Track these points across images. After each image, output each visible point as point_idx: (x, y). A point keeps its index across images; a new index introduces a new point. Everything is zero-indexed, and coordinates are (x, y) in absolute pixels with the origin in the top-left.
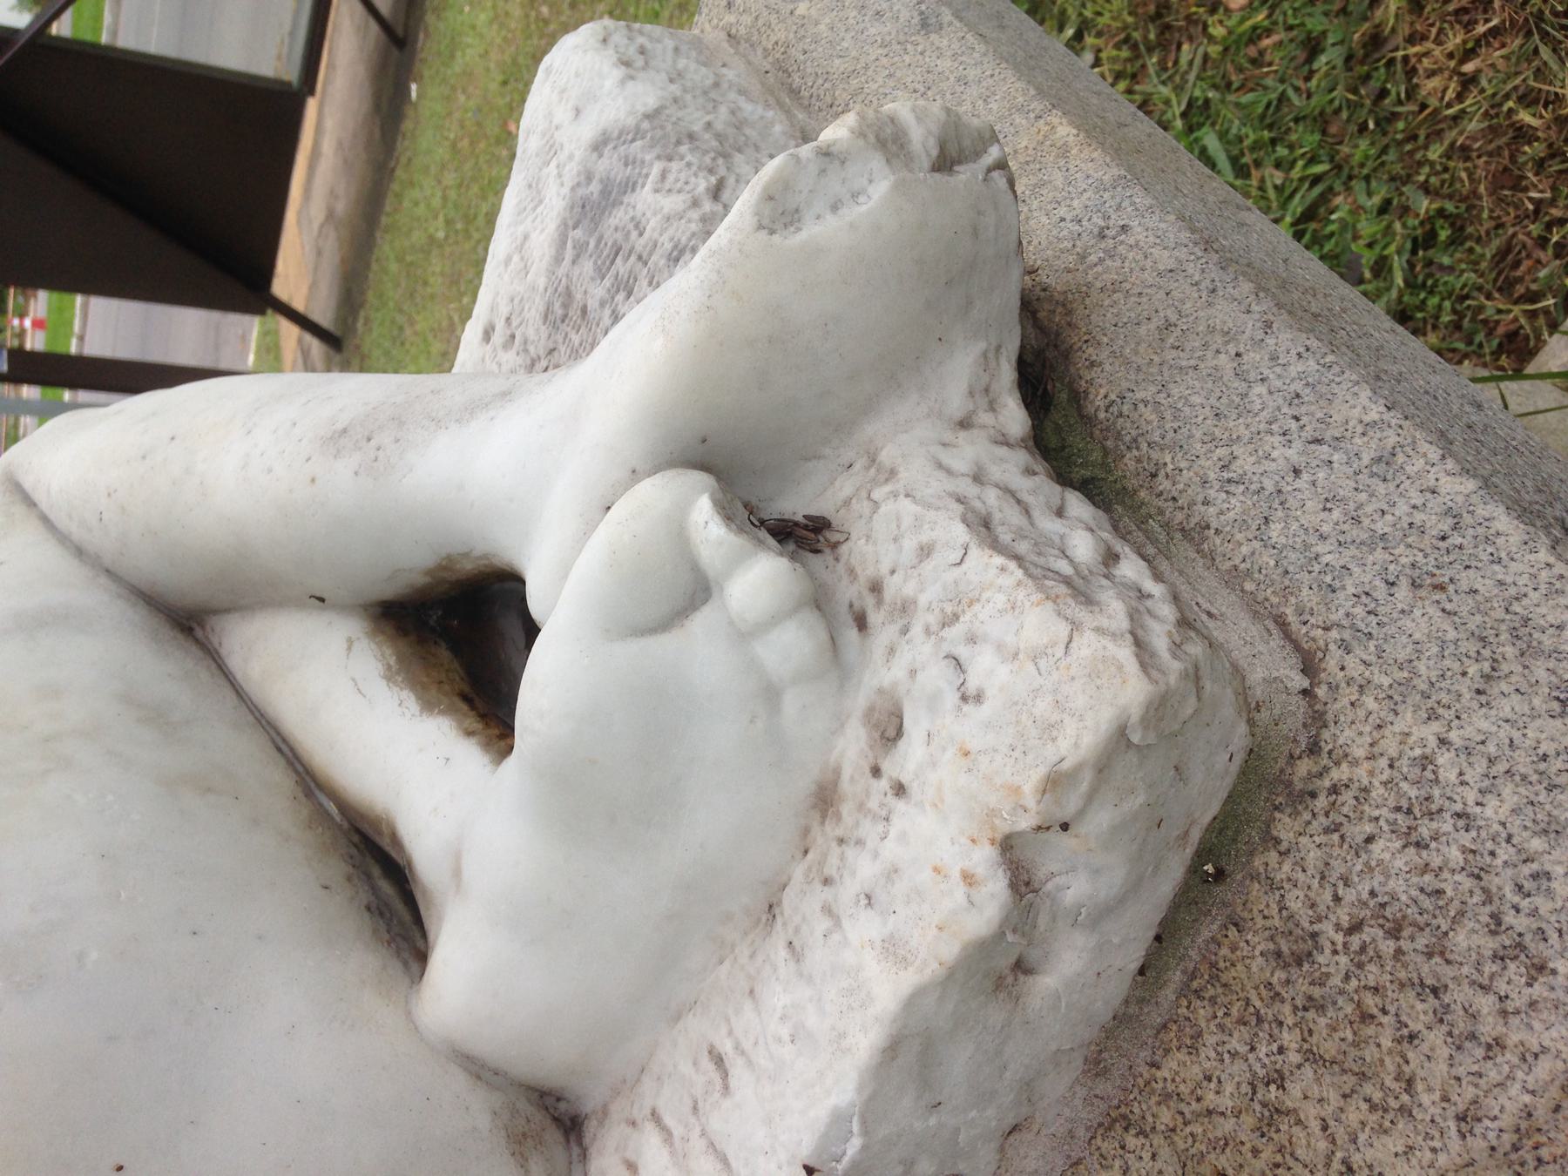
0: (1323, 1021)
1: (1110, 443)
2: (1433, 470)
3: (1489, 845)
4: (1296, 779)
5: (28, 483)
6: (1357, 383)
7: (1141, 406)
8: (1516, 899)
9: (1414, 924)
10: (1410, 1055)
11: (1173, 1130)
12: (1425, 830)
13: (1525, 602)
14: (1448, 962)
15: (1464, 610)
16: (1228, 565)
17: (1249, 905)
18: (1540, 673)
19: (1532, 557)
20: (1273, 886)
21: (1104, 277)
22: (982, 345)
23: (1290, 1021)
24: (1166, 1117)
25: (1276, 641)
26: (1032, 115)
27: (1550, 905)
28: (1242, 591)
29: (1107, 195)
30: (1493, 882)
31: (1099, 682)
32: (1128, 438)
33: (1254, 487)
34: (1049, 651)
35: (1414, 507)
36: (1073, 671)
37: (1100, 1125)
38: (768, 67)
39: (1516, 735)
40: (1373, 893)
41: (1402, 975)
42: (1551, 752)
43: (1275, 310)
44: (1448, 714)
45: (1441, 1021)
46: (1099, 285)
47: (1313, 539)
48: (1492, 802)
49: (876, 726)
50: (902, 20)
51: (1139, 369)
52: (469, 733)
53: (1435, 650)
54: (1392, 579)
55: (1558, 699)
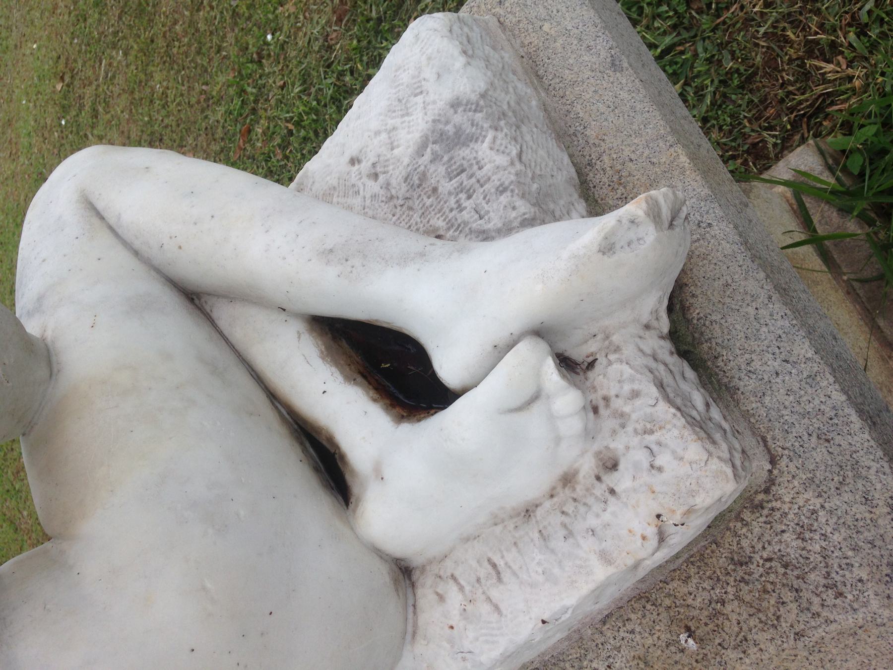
0: (747, 588)
1: (696, 335)
2: (830, 387)
3: (832, 549)
4: (756, 500)
5: (100, 206)
6: (804, 337)
7: (714, 323)
8: (838, 570)
9: (795, 566)
10: (781, 609)
11: (670, 607)
12: (807, 535)
13: (858, 454)
14: (805, 582)
15: (836, 453)
16: (745, 408)
17: (724, 539)
18: (860, 486)
19: (862, 435)
20: (736, 534)
21: (700, 249)
22: (661, 293)
23: (732, 584)
24: (667, 602)
25: (762, 448)
26: (668, 144)
27: (851, 576)
28: (749, 421)
29: (702, 203)
30: (830, 562)
31: (717, 480)
32: (707, 337)
33: (760, 377)
34: (698, 462)
35: (821, 402)
36: (708, 473)
37: (634, 597)
38: (523, 54)
39: (848, 509)
40: (780, 550)
41: (785, 581)
42: (860, 519)
43: (773, 290)
44: (826, 496)
45: (797, 601)
46: (697, 253)
47: (782, 407)
48: (837, 535)
49: (601, 460)
50: (601, 57)
51: (714, 305)
52: (375, 400)
53: (823, 468)
54: (810, 433)
55: (864, 497)
